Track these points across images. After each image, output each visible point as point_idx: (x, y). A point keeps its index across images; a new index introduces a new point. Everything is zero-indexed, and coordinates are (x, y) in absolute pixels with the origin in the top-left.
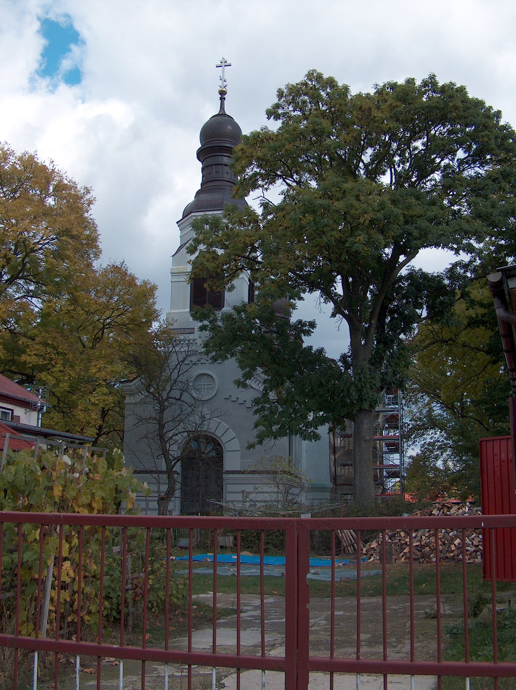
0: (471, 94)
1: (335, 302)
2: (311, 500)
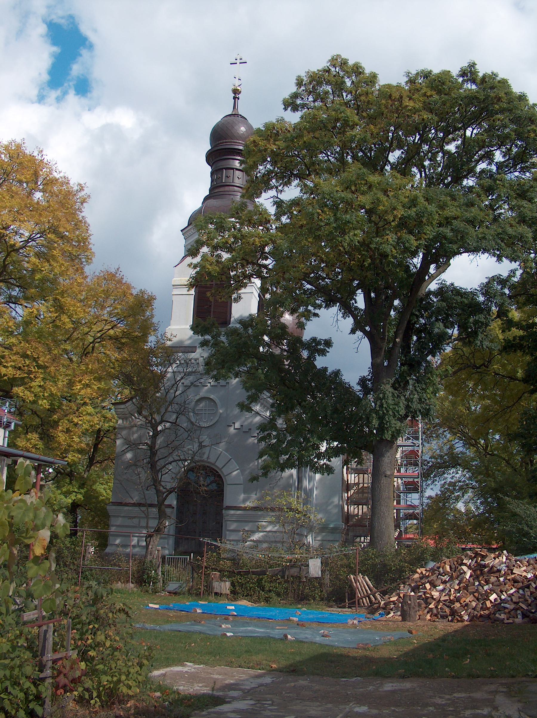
0: (516, 89)
1: (355, 317)
2: (320, 542)
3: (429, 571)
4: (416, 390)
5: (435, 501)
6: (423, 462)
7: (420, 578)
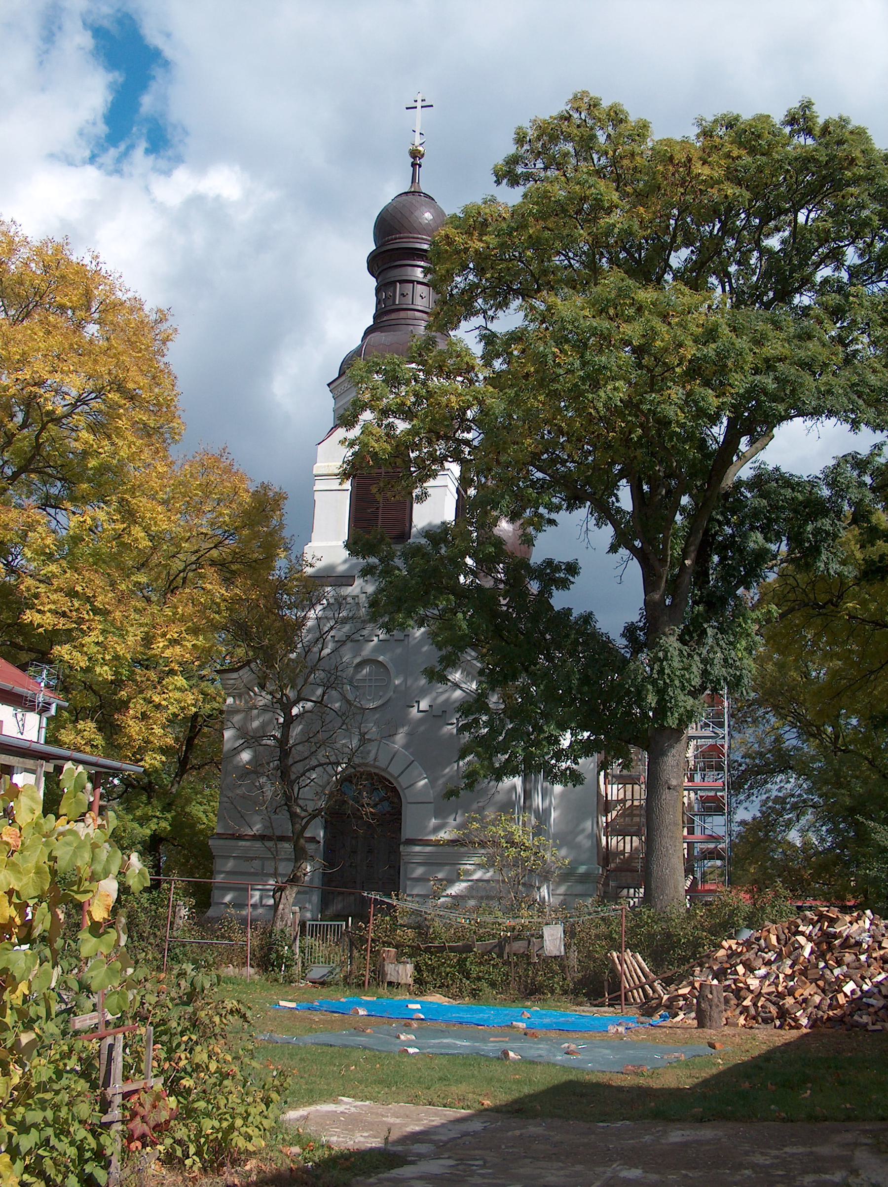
3: (742, 944)
4: (718, 645)
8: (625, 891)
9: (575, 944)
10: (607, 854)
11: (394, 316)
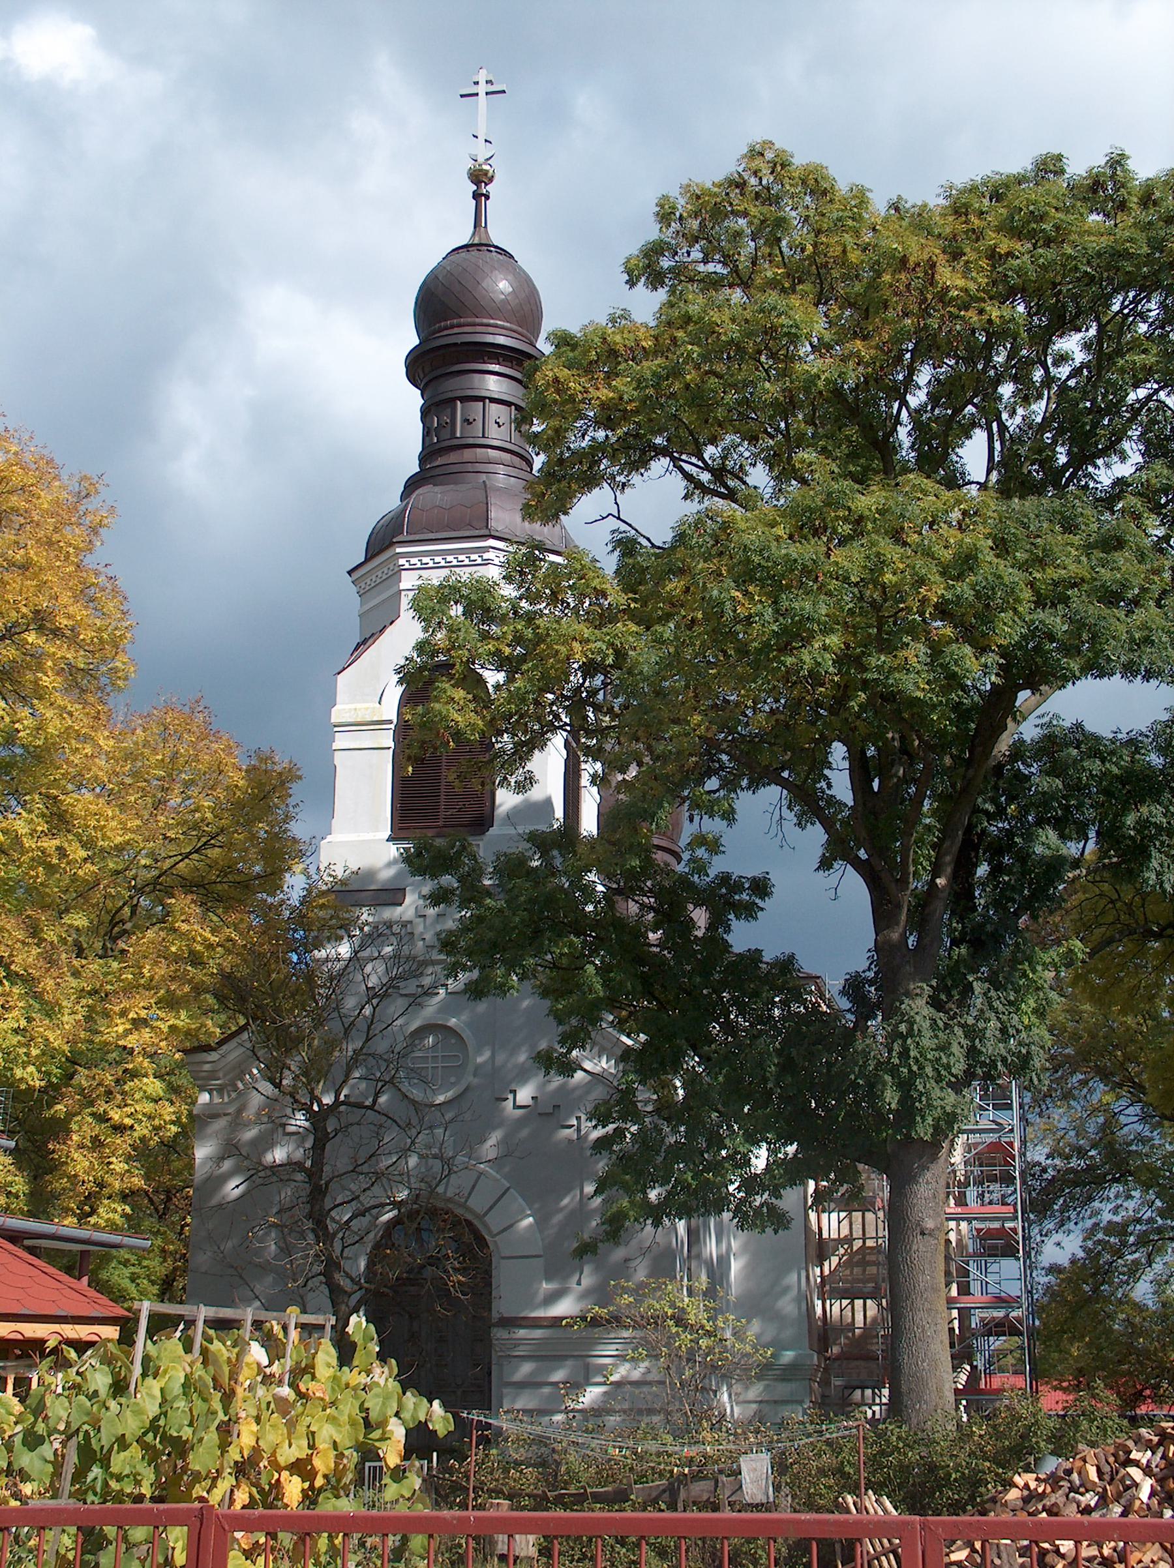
1: (827, 825)
3: (1044, 1480)
4: (991, 1007)
5: (1069, 1280)
6: (1029, 1169)
7: (1022, 1499)
8: (858, 1392)
9: (787, 1484)
10: (825, 1331)
11: (453, 457)
